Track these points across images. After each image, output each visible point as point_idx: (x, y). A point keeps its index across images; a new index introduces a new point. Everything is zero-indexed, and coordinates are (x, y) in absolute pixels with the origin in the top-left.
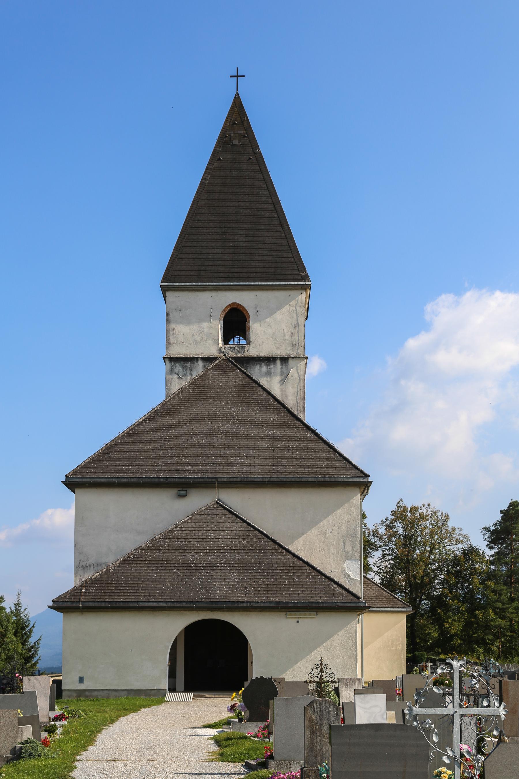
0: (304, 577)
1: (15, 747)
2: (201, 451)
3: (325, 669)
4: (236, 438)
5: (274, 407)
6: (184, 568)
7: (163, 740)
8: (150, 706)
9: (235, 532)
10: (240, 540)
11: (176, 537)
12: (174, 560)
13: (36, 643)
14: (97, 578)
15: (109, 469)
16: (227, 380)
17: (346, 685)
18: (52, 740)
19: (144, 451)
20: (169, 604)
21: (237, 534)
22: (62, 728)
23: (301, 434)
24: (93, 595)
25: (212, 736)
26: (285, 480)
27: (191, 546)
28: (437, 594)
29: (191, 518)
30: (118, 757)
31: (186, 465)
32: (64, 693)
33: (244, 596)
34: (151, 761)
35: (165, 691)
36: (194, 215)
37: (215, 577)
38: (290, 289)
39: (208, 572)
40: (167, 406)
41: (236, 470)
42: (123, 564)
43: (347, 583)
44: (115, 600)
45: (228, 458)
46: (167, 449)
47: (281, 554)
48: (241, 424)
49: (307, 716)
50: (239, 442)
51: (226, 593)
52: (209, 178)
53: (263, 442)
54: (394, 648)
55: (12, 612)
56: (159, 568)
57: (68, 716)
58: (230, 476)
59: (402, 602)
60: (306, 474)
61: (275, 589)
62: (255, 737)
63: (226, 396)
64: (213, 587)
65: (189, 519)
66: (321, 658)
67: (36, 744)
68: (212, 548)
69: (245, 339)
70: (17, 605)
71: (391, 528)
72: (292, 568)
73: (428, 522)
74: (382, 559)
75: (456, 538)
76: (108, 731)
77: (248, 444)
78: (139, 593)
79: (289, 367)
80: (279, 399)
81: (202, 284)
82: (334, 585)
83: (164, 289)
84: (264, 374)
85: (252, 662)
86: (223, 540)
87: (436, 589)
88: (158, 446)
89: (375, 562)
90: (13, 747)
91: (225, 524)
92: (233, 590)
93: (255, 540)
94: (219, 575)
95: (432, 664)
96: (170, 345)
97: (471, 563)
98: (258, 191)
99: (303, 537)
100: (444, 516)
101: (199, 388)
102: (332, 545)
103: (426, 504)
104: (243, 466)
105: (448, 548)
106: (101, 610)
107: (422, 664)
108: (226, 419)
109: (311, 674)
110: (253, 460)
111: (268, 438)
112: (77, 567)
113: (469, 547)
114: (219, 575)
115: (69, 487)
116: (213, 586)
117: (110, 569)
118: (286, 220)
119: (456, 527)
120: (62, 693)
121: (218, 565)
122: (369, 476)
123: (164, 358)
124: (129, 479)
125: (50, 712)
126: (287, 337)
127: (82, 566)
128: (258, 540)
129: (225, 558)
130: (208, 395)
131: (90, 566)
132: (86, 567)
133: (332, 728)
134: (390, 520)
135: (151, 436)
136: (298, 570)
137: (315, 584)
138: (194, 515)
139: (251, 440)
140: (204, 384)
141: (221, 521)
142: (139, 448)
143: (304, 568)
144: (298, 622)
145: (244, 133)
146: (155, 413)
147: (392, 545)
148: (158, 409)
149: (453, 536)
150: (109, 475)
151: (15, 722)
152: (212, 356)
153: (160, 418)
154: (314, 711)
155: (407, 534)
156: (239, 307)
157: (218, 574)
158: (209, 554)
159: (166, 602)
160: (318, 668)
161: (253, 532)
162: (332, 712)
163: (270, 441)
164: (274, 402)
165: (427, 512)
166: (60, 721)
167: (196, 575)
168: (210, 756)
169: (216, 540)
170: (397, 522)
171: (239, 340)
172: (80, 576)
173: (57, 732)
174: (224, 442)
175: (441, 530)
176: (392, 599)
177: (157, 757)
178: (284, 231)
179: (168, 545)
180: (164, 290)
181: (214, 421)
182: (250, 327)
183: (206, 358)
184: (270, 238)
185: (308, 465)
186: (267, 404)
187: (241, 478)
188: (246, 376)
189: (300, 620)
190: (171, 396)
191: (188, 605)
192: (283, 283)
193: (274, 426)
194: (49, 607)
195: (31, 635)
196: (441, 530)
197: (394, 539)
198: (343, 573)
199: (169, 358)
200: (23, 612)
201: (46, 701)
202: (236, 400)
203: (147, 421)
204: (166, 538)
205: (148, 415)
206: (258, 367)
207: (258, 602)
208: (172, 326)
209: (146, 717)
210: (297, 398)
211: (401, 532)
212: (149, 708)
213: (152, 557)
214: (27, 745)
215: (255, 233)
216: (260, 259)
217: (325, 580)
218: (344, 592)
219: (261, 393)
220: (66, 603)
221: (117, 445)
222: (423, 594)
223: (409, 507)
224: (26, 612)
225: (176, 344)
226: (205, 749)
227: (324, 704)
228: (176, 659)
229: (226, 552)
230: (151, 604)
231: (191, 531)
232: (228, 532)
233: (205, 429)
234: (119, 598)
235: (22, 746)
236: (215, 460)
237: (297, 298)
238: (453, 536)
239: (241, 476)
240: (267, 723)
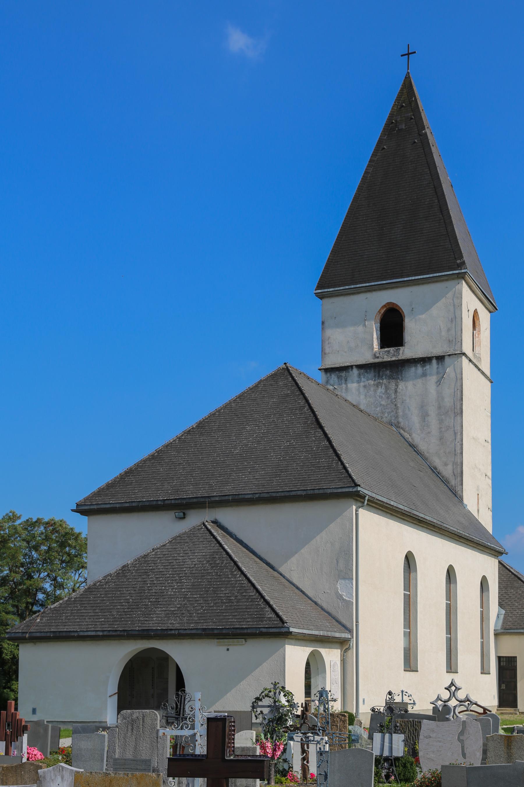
20: (105, 633)
26: (274, 495)
36: (353, 213)
38: (447, 280)
42: (86, 592)
43: (340, 605)
50: (251, 457)
65: (168, 543)
81: (355, 286)
82: (268, 609)
93: (218, 562)
98: (420, 176)
99: (296, 555)
102: (325, 563)
124: (131, 503)
126: (443, 333)
138: (175, 538)
144: (228, 650)
156: (395, 307)
159: (103, 631)
178: (443, 216)
183: (360, 365)
187: (232, 496)
189: (230, 648)
191: (122, 633)
192: (438, 274)
198: (336, 594)
205: (181, 435)
206: (413, 369)
207: (186, 629)
208: (329, 332)
210: (454, 400)
220: (17, 634)
225: (331, 353)
230: (90, 633)
237: (454, 289)
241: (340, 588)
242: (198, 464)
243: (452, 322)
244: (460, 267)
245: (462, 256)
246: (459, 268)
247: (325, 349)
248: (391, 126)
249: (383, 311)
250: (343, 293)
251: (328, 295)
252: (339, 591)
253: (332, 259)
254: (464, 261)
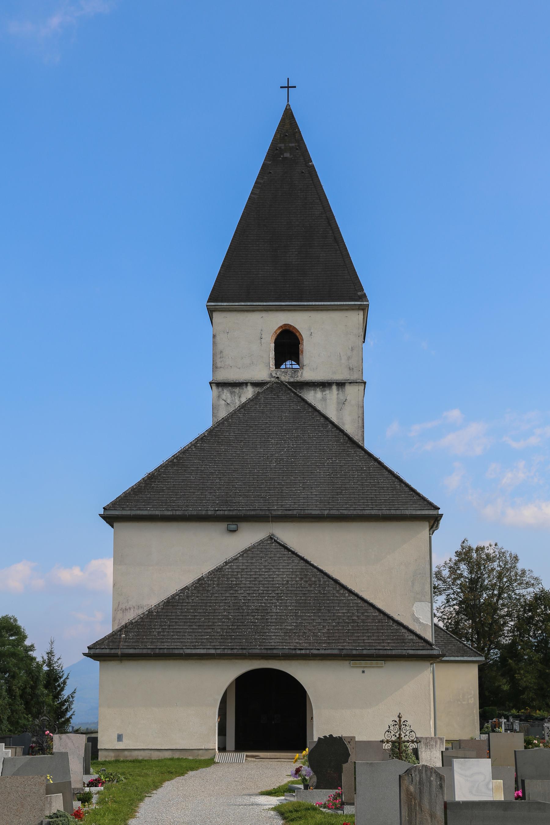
0: (369, 620)
2: (253, 482)
3: (404, 726)
6: (235, 611)
7: (217, 811)
8: (198, 768)
9: (291, 570)
10: (298, 579)
11: (226, 576)
12: (224, 601)
14: (138, 622)
15: (151, 501)
16: (280, 405)
17: (426, 744)
18: (86, 812)
19: (190, 481)
22: (97, 795)
24: (134, 641)
25: (274, 805)
27: (243, 586)
28: (507, 642)
29: (243, 554)
31: (237, 496)
33: (303, 643)
35: (214, 751)
37: (269, 620)
39: (262, 616)
40: (215, 433)
41: (291, 502)
44: (158, 647)
46: (215, 479)
48: (296, 452)
49: (404, 787)
50: (295, 472)
51: (283, 639)
53: (321, 471)
54: (465, 703)
55: (44, 662)
57: (105, 780)
59: (474, 651)
61: (337, 635)
62: (325, 808)
63: (279, 421)
64: (267, 632)
65: (240, 556)
66: (400, 714)
67: (68, 817)
69: (298, 364)
70: (50, 653)
71: (456, 570)
72: (356, 611)
73: (496, 564)
74: (446, 603)
75: (527, 581)
77: (305, 474)
79: (345, 393)
82: (404, 631)
83: (211, 309)
84: (318, 400)
85: (312, 718)
87: (506, 637)
89: (439, 607)
90: (39, 822)
91: (280, 561)
92: (290, 636)
93: (313, 579)
94: (274, 619)
95: (505, 720)
97: (544, 608)
105: (517, 592)
107: (494, 720)
109: (388, 732)
110: (310, 491)
111: (327, 467)
112: (115, 610)
113: (541, 591)
114: (274, 619)
115: (108, 520)
116: (267, 631)
117: (152, 612)
118: (342, 237)
119: (526, 569)
120: (98, 752)
121: (273, 607)
122: (439, 509)
123: (210, 383)
128: (317, 579)
129: (281, 600)
131: (130, 608)
133: (448, 806)
134: (454, 561)
135: (197, 465)
140: (255, 409)
141: (276, 558)
142: (185, 478)
143: (370, 611)
144: (363, 672)
145: (295, 146)
146: (202, 439)
148: (205, 436)
149: (523, 579)
150: (152, 508)
151: (43, 790)
152: (262, 381)
153: (207, 445)
154: (412, 781)
155: (472, 576)
156: (291, 329)
157: (273, 617)
158: (263, 595)
162: (434, 783)
164: (332, 428)
165: (494, 553)
166: (96, 786)
169: (271, 579)
171: (292, 364)
172: (119, 620)
174: (278, 472)
175: (510, 573)
179: (217, 585)
180: (210, 311)
181: (267, 448)
182: (303, 350)
183: (256, 383)
184: (324, 255)
186: (325, 430)
189: (365, 669)
194: (84, 654)
195: (65, 687)
196: (510, 573)
197: (459, 582)
199: (216, 383)
201: (79, 763)
202: (290, 426)
204: (214, 577)
205: (194, 442)
211: (466, 574)
212: (196, 770)
213: (200, 598)
214: (56, 819)
215: (308, 250)
217: (393, 624)
219: (318, 418)
221: (161, 474)
222: (492, 642)
223: (474, 547)
224: (59, 662)
227: (424, 772)
228: (226, 714)
229: (282, 593)
231: (242, 569)
232: (284, 570)
233: (257, 458)
234: (162, 644)
235: (51, 820)
236: (269, 491)
238: (523, 579)
239: (298, 509)
240: (337, 790)
241: (416, 611)
248: (275, 152)
252: (415, 614)
253: (223, 274)
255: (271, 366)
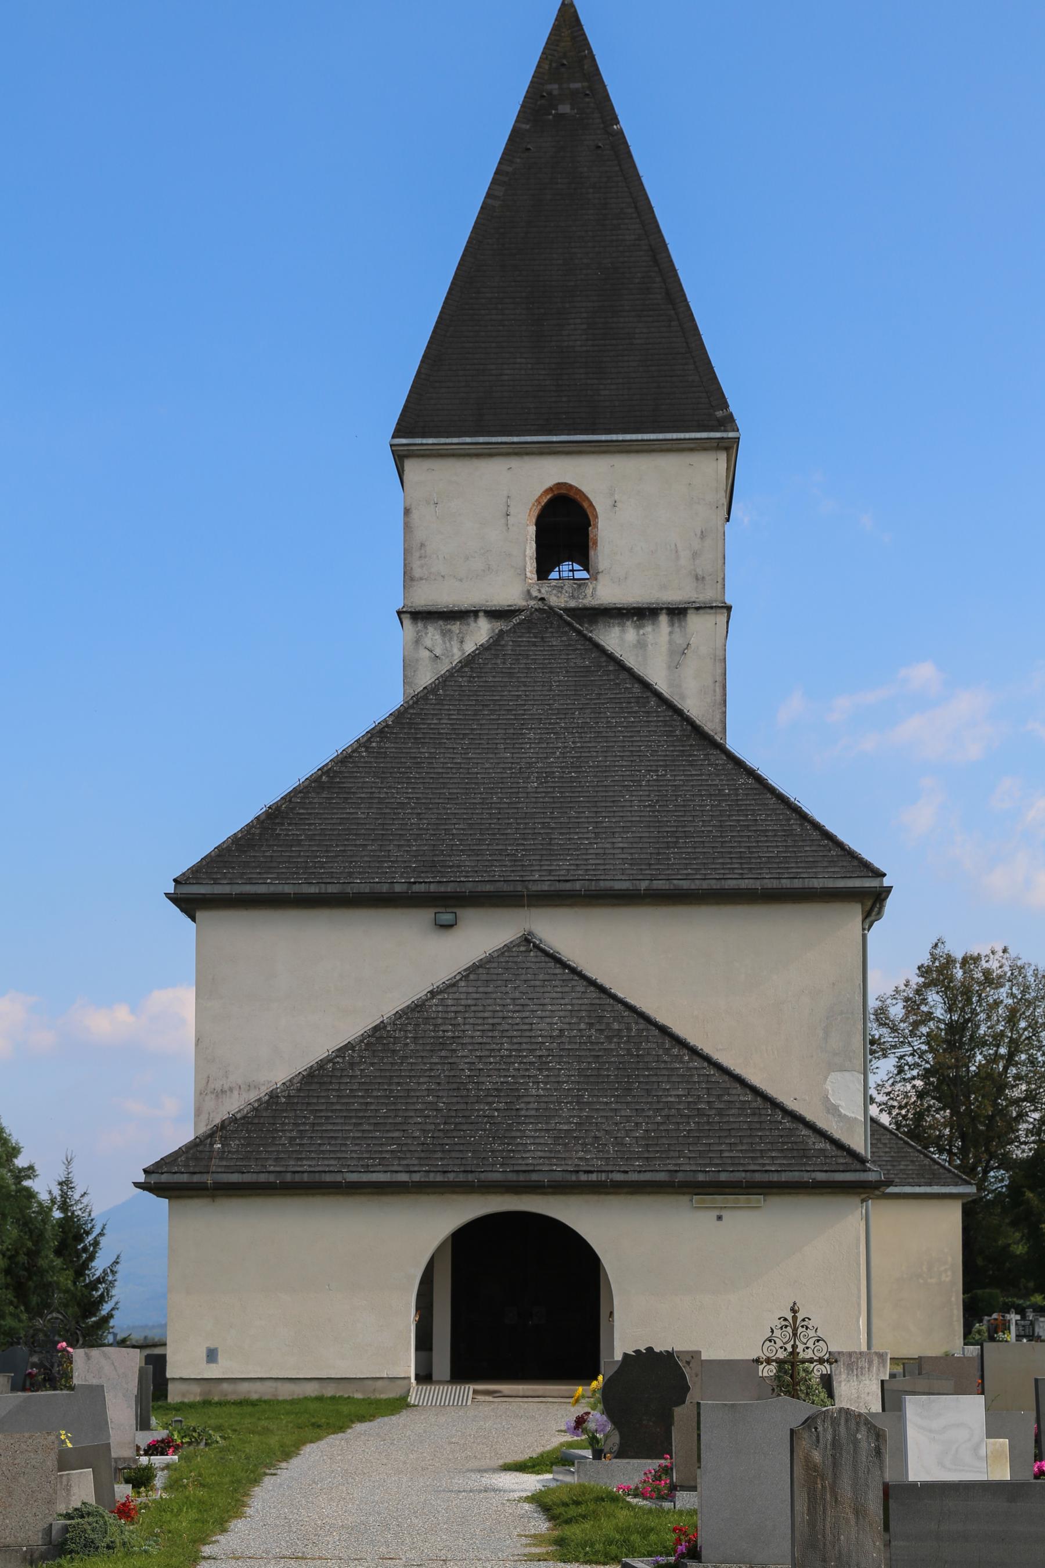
0: (733, 1111)
1: (51, 1525)
2: (490, 821)
3: (804, 1329)
4: (569, 789)
5: (659, 716)
6: (451, 1093)
7: (412, 1504)
8: (374, 1417)
9: (570, 1007)
10: (583, 1026)
11: (431, 1021)
12: (427, 1074)
13: (109, 1271)
14: (249, 1117)
15: (274, 864)
16: (547, 657)
17: (850, 1367)
21: (573, 1013)
23: (723, 780)
24: (240, 1156)
30: (304, 1549)
32: (171, 1387)
33: (593, 1158)
34: (386, 1559)
35: (406, 1381)
37: (523, 1113)
40: (410, 719)
41: (570, 865)
45: (553, 837)
47: (678, 1058)
48: (581, 757)
49: (800, 1454)
50: (578, 800)
51: (550, 1151)
52: (502, 194)
54: (933, 1281)
55: (53, 1201)
56: (393, 1092)
57: (182, 1442)
58: (557, 878)
60: (736, 871)
61: (665, 1141)
62: (635, 1496)
64: (518, 1137)
65: (461, 979)
66: (795, 1304)
67: (103, 1517)
68: (516, 1047)
70: (66, 1184)
71: (918, 1005)
73: (1003, 991)
76: (278, 1480)
78: (346, 1152)
80: (669, 697)
82: (805, 1132)
85: (611, 1314)
86: (543, 1028)
88: (388, 811)
89: (881, 1083)
90: (45, 1526)
91: (546, 990)
92: (566, 1145)
93: (616, 1026)
95: (1018, 1317)
96: (415, 583)
100: (1039, 976)
101: (483, 675)
103: (999, 949)
104: (587, 854)
106: (259, 1191)
108: (545, 745)
110: (610, 840)
111: (646, 788)
112: (201, 1094)
115: (184, 906)
116: (518, 1134)
117: (278, 1097)
120: (167, 1385)
121: (531, 1084)
122: (884, 875)
125: (139, 1433)
127: (212, 1090)
128: (622, 1026)
129: (548, 1069)
130: (504, 691)
131: (231, 1089)
132: (223, 1092)
134: (915, 987)
135: (372, 788)
136: (719, 1096)
137: (760, 1129)
139: (604, 794)
141: (538, 983)
142: (345, 816)
143: (734, 1092)
144: (720, 1218)
146: (380, 732)
147: (921, 1043)
150: (276, 879)
151: (51, 1462)
153: (393, 745)
154: (818, 1441)
155: (953, 1018)
156: (572, 494)
157: (531, 1106)
158: (508, 1060)
160: (786, 1326)
161: (613, 1007)
162: (864, 1445)
163: (649, 796)
164: (658, 706)
165: (1001, 967)
167: (478, 1110)
168: (530, 1545)
170: (931, 990)
171: (573, 571)
173: (155, 1482)
174: (541, 800)
175: (1034, 1009)
176: (930, 1165)
177: (402, 1549)
180: (399, 456)
181: (520, 750)
182: (597, 539)
183: (496, 611)
184: (645, 330)
185: (741, 852)
186: (643, 709)
188: (591, 647)
189: (725, 1214)
190: (417, 694)
193: (658, 761)
194: (137, 1185)
195: (96, 1252)
196: (1034, 1009)
197: (924, 1030)
199: (411, 613)
200: (78, 1202)
201: (128, 1407)
202: (569, 702)
203: (362, 752)
204: (407, 1024)
205: (365, 739)
209: (365, 1444)
211: (939, 1012)
212: (370, 1421)
213: (377, 1067)
214: (80, 1520)
216: (621, 381)
217: (783, 1118)
218: (829, 1148)
219: (628, 686)
221: (294, 808)
222: (992, 1156)
223: (959, 956)
224: (85, 1200)
226: (515, 1528)
227: (843, 1422)
228: (432, 1305)
229: (549, 1056)
231: (466, 1006)
232: (554, 1008)
233: (499, 771)
234: (299, 1163)
235: (68, 1522)
236: (522, 842)
239: (583, 878)
242: (451, 808)
243: (702, 539)
244: (724, 426)
245: (727, 402)
246: (722, 428)
247: (412, 569)
248: (539, 103)
249: (545, 501)
250: (456, 451)
251: (422, 452)
252: (829, 1096)
254: (731, 415)
255: (529, 574)
